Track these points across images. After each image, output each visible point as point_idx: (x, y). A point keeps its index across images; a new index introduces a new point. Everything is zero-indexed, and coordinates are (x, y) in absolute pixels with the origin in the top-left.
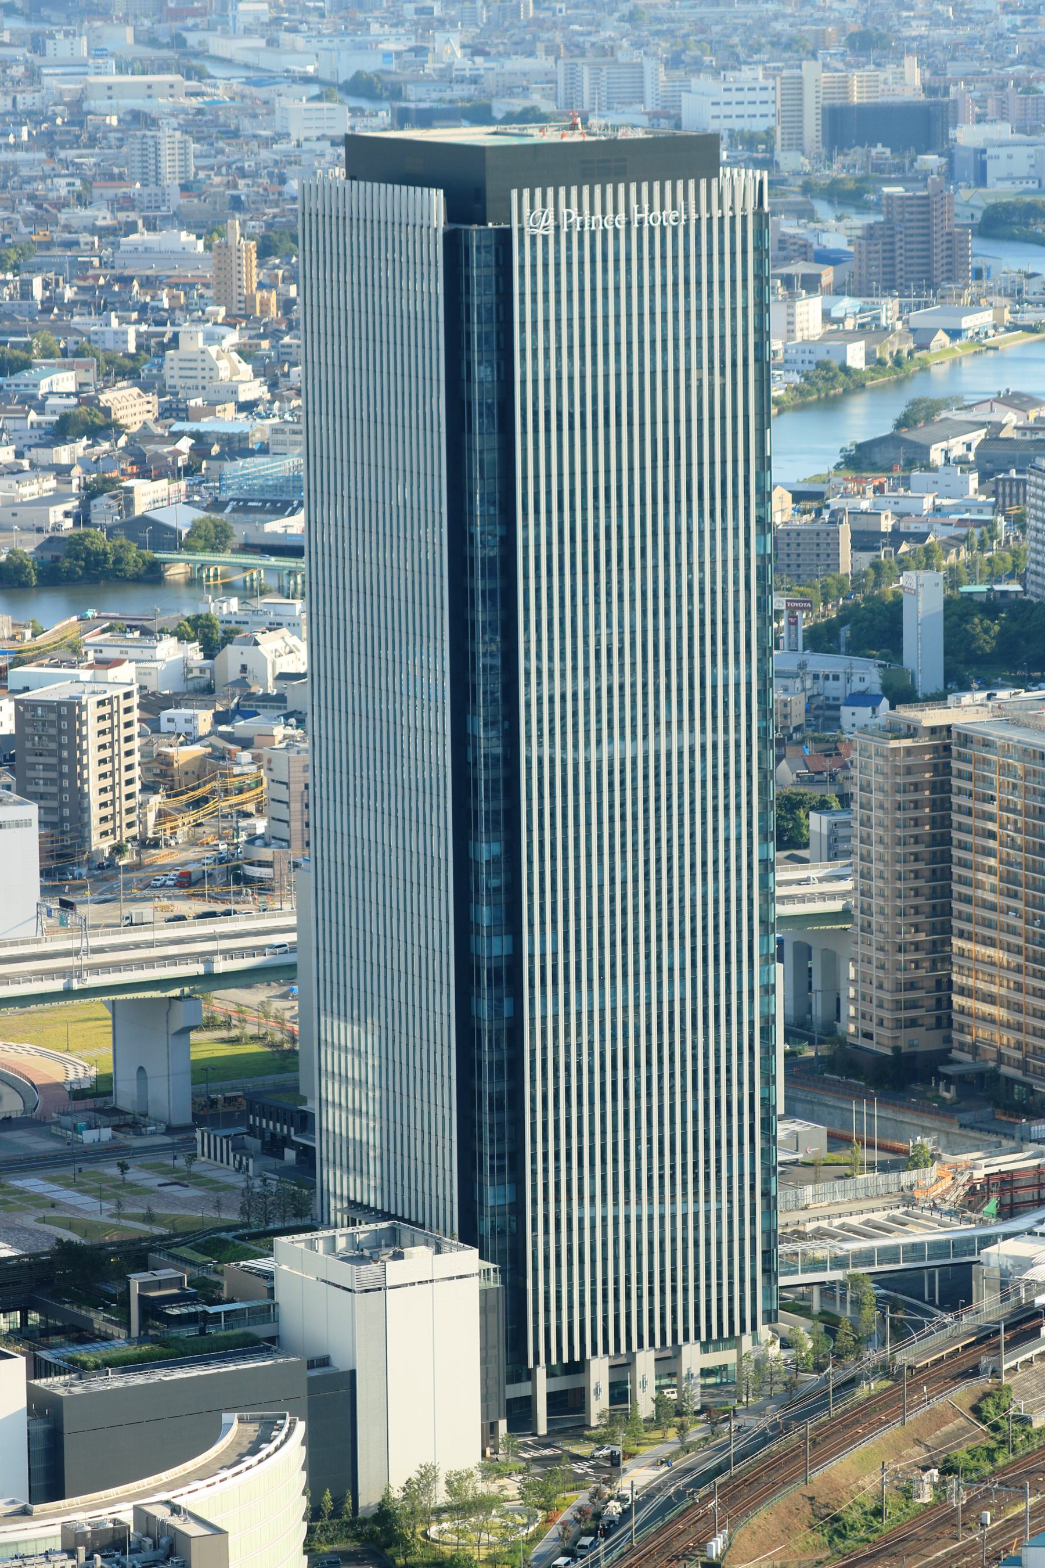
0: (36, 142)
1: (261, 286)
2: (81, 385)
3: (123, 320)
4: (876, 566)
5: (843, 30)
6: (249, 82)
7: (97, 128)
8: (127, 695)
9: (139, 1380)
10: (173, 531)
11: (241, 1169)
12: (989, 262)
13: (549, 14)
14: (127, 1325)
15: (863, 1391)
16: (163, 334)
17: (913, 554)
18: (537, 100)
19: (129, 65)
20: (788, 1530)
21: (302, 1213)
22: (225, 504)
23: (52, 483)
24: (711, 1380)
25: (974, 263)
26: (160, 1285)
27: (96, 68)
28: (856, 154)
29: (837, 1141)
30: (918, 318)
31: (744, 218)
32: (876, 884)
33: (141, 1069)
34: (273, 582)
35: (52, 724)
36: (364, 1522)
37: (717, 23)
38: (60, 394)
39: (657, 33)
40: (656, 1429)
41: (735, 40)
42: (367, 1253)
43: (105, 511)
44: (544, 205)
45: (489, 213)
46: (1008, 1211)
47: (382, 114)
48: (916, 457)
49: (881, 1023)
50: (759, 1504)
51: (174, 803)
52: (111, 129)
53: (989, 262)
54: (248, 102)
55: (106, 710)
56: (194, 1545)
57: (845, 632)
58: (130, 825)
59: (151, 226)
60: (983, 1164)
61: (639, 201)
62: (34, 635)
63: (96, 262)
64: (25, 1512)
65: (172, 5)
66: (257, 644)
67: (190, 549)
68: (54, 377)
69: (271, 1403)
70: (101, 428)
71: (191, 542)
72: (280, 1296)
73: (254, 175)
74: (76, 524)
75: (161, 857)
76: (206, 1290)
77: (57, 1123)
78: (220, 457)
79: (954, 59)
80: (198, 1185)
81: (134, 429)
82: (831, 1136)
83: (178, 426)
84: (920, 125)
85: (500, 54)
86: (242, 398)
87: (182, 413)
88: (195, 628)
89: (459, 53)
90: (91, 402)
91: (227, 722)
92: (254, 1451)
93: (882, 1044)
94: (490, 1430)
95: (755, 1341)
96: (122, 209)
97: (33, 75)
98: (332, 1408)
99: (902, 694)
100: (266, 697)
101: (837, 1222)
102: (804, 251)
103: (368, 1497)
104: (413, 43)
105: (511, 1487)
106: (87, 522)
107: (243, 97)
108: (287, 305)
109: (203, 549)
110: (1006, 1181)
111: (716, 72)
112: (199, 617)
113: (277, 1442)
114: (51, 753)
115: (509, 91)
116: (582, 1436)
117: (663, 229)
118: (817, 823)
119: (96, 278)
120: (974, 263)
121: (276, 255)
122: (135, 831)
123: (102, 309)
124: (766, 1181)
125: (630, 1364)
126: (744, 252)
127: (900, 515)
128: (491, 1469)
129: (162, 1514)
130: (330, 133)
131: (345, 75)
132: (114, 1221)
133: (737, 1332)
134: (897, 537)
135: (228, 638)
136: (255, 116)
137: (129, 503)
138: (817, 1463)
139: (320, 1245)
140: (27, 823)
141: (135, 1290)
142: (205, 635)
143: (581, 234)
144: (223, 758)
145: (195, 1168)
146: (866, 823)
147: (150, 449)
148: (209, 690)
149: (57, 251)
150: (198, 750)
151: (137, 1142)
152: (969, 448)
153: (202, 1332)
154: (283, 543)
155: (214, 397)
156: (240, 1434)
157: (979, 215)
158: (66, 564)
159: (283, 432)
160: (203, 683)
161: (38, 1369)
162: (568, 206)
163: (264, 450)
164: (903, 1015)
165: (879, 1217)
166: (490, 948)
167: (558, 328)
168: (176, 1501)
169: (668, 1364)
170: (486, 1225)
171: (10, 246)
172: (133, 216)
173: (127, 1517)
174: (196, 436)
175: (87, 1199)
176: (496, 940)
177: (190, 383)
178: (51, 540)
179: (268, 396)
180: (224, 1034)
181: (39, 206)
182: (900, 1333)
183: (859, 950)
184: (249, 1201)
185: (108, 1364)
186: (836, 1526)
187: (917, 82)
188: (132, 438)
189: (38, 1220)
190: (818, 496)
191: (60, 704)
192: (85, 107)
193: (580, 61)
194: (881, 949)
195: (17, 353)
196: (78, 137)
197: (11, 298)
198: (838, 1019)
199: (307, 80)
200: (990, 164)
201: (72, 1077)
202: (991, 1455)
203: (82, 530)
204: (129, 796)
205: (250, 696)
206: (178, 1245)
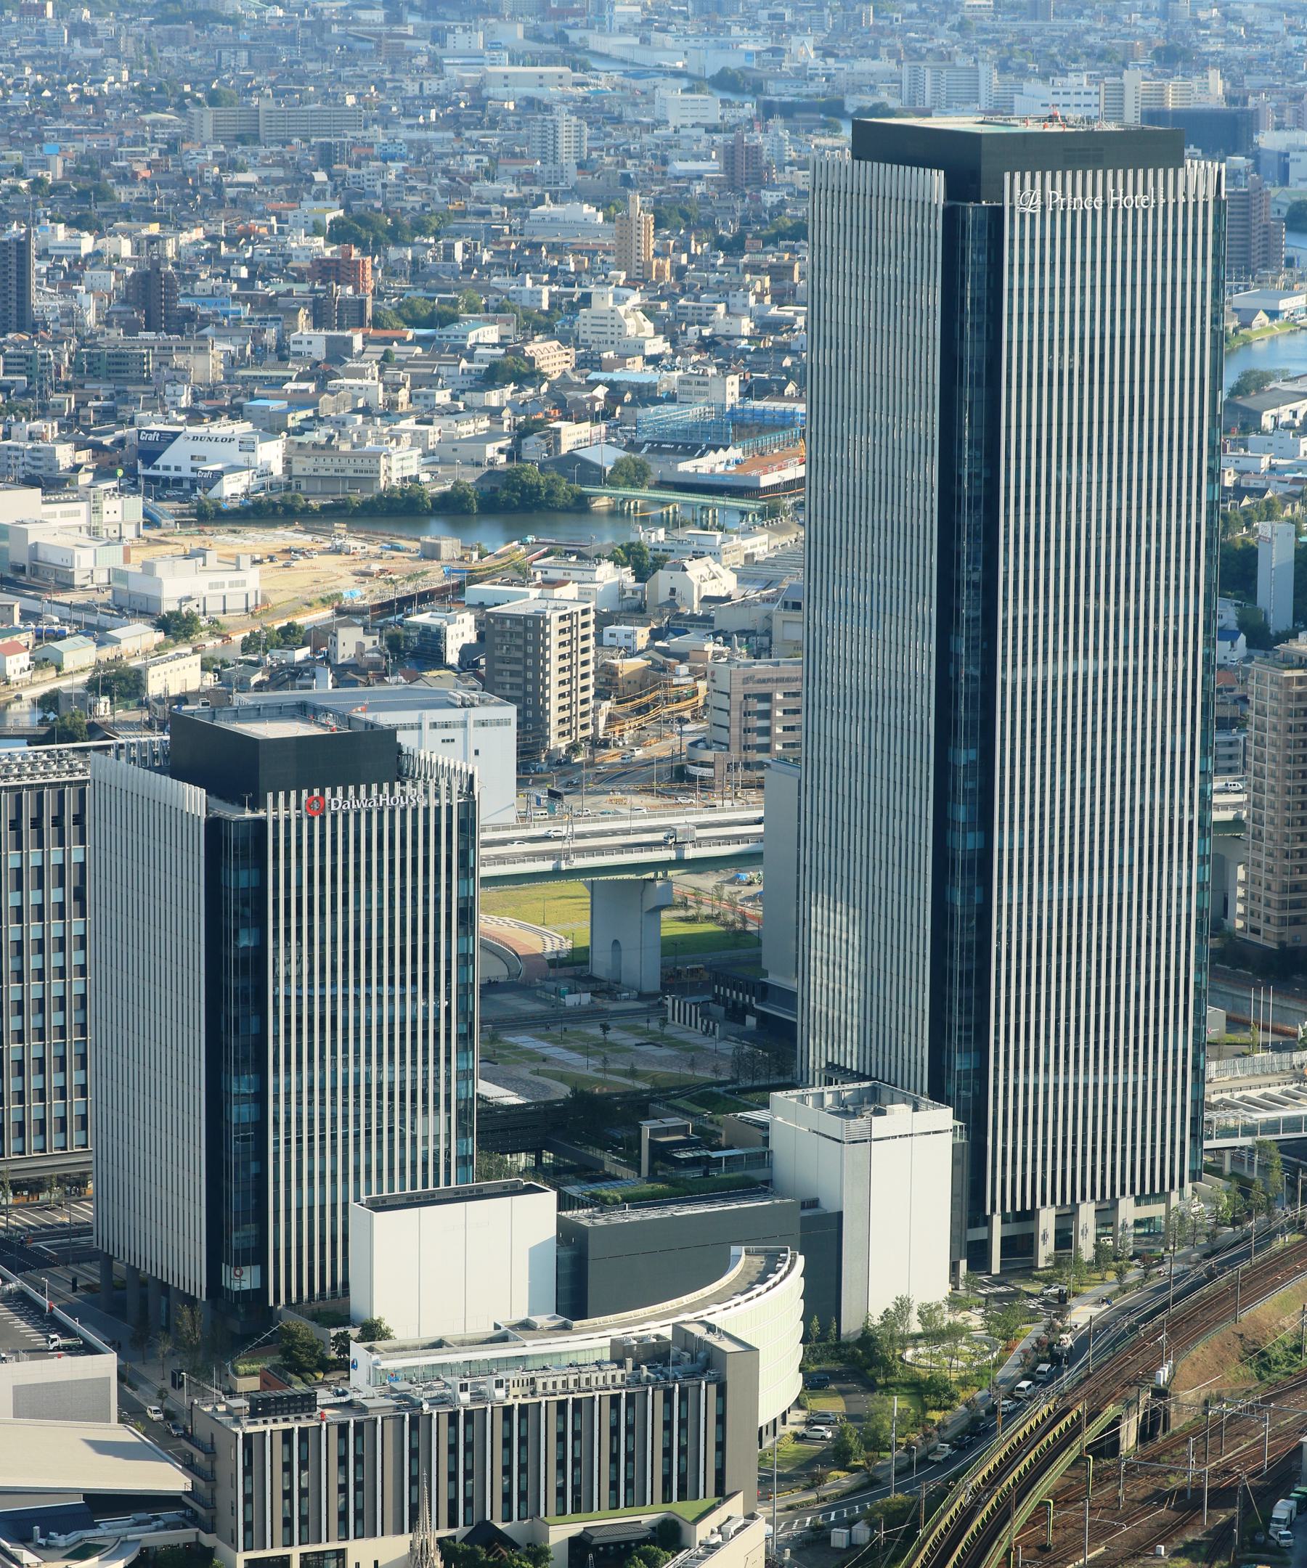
0: (443, 123)
1: (656, 254)
2: (502, 337)
3: (536, 282)
5: (1149, 44)
6: (626, 74)
7: (497, 112)
8: (585, 612)
9: (653, 1214)
10: (600, 469)
12: (1299, 252)
13: (887, 22)
14: (638, 1168)
15: (1280, 1243)
16: (572, 294)
17: (1256, 507)
18: (884, 97)
19: (520, 57)
20: (1222, 1363)
22: (640, 446)
23: (486, 423)
24: (1140, 1231)
26: (668, 1131)
27: (491, 58)
31: (1206, 204)
33: (616, 942)
34: (689, 516)
35: (518, 635)
36: (847, 1345)
37: (1036, 35)
38: (487, 345)
39: (985, 42)
40: (1097, 1270)
41: (1054, 50)
42: (850, 1108)
43: (534, 448)
44: (1033, 187)
45: (983, 193)
47: (748, 105)
49: (1268, 920)
50: (1196, 1340)
51: (621, 709)
52: (508, 113)
53: (1299, 252)
54: (628, 92)
55: (567, 624)
56: (729, 1359)
58: (584, 727)
61: (1115, 186)
62: (481, 557)
63: (506, 229)
64: (565, 1327)
65: (554, 6)
66: (685, 569)
67: (614, 484)
68: (480, 330)
70: (526, 376)
71: (614, 478)
72: (773, 1145)
73: (640, 156)
74: (509, 459)
75: (610, 757)
76: (707, 1138)
77: (542, 988)
78: (633, 403)
79: (1249, 73)
80: (671, 1045)
81: (556, 376)
82: (1228, 1019)
83: (594, 376)
85: (847, 57)
86: (648, 352)
87: (598, 365)
88: (628, 554)
89: (812, 55)
90: (517, 352)
91: (662, 639)
92: (763, 1280)
93: (1269, 938)
94: (954, 1267)
95: (1181, 1197)
96: (525, 184)
97: (436, 66)
98: (821, 1241)
100: (693, 617)
101: (1238, 1095)
103: (850, 1325)
104: (769, 45)
106: (519, 459)
107: (623, 88)
108: (679, 272)
109: (625, 485)
111: (1045, 77)
112: (631, 545)
113: (781, 1273)
114: (517, 661)
115: (858, 88)
116: (1031, 1276)
117: (1135, 211)
119: (509, 243)
120: (1287, 252)
121: (666, 227)
122: (590, 731)
123: (517, 272)
124: (1196, 1056)
125: (1074, 1213)
126: (1205, 234)
127: (1242, 473)
129: (699, 1331)
130: (703, 121)
131: (712, 70)
132: (600, 1075)
133: (1167, 1189)
135: (659, 563)
136: (636, 105)
137: (558, 442)
139: (810, 1100)
140: (507, 722)
141: (646, 1135)
142: (636, 561)
143: (1064, 214)
144: (664, 670)
145: (668, 1030)
146: (1260, 742)
149: (471, 219)
150: (638, 663)
151: (613, 1007)
152: (1295, 415)
153: (706, 1174)
154: (694, 481)
155: (624, 351)
156: (747, 1265)
157: (1285, 211)
158: (504, 495)
159: (689, 383)
160: (635, 603)
161: (565, 1203)
162: (1053, 188)
163: (672, 399)
164: (1288, 913)
165: (1274, 1091)
166: (965, 842)
167: (1194, 289)
168: (709, 1319)
169: (1106, 1215)
170: (951, 1088)
171: (431, 213)
172: (537, 190)
173: (667, 1333)
174: (611, 385)
175: (573, 1055)
176: (970, 836)
177: (602, 337)
178: (490, 473)
179: (670, 351)
180: (682, 913)
181: (453, 180)
183: (1250, 854)
184: (739, 1063)
185: (626, 1199)
186: (1263, 1361)
187: (1220, 92)
188: (552, 385)
189: (533, 1073)
191: (527, 617)
192: (484, 93)
193: (922, 64)
194: (1270, 855)
195: (446, 307)
196: (480, 119)
197: (435, 259)
198: (1225, 915)
199: (678, 74)
200: (1292, 166)
201: (549, 949)
203: (515, 465)
204: (584, 702)
205: (679, 616)
206: (675, 1097)
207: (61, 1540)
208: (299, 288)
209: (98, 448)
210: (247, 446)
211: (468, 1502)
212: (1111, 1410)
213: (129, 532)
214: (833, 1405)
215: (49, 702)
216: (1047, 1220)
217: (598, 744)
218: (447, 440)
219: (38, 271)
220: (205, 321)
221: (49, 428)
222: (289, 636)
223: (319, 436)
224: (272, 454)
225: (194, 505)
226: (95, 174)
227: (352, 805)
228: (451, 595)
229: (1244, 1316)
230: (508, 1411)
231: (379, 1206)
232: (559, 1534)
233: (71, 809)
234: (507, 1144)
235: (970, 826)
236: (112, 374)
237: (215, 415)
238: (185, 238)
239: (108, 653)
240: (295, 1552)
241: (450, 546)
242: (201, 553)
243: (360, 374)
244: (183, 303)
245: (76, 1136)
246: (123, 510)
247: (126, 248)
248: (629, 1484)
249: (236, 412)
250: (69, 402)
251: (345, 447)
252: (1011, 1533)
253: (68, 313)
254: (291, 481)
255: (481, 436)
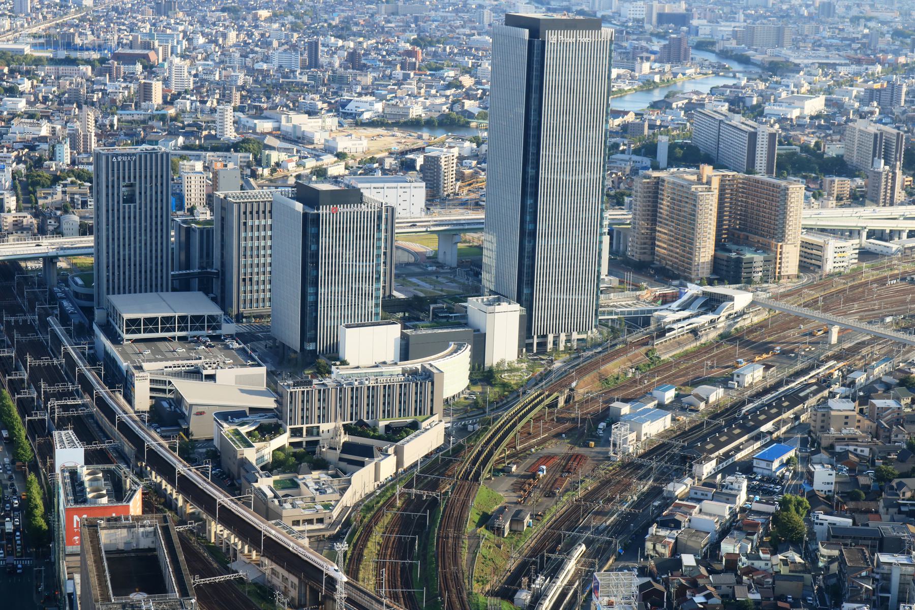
4: (654, 134)
11: (468, 279)
15: (618, 347)
21: (477, 291)
25: (691, 56)
28: (665, 26)
29: (621, 282)
30: (675, 69)
32: (637, 217)
43: (457, 108)
46: (663, 303)
48: (669, 106)
57: (643, 150)
59: (479, 34)
60: (659, 290)
64: (396, 364)
69: (464, 340)
72: (468, 313)
84: (682, 19)
90: (457, 79)
93: (636, 258)
94: (520, 352)
98: (479, 343)
99: (656, 168)
102: (647, 51)
105: (524, 365)
110: (664, 295)
118: (627, 200)
120: (691, 56)
125: (559, 336)
127: (662, 121)
128: (520, 361)
129: (428, 367)
134: (660, 126)
137: (463, 106)
138: (603, 365)
147: (471, 92)
148: (477, 155)
151: (442, 271)
161: (404, 327)
165: (630, 303)
166: (529, 227)
174: (483, 90)
182: (629, 332)
190: (642, 115)
202: (649, 366)
207: (237, 421)
208: (398, 58)
209: (330, 103)
210: (371, 104)
211: (356, 414)
212: (555, 394)
213: (334, 128)
214: (478, 389)
215: (298, 177)
216: (550, 338)
217: (456, 194)
218: (432, 104)
219: (322, 51)
220: (369, 67)
221: (317, 97)
222: (372, 160)
223: (393, 102)
224: (379, 107)
225: (351, 119)
226: (348, 22)
227: (345, 210)
228: (421, 150)
229: (602, 368)
230: (369, 387)
231: (348, 327)
232: (382, 424)
233: (268, 209)
234: (390, 309)
235: (530, 222)
236: (339, 81)
237: (366, 95)
238: (369, 42)
239: (319, 163)
240: (305, 426)
241: (426, 135)
242: (351, 135)
243: (410, 84)
244: (363, 61)
245: (268, 304)
246: (331, 121)
247: (352, 45)
248: (404, 410)
249: (372, 94)
250: (324, 90)
251: (401, 105)
252: (519, 427)
253: (330, 63)
254: (384, 115)
255: (441, 104)
